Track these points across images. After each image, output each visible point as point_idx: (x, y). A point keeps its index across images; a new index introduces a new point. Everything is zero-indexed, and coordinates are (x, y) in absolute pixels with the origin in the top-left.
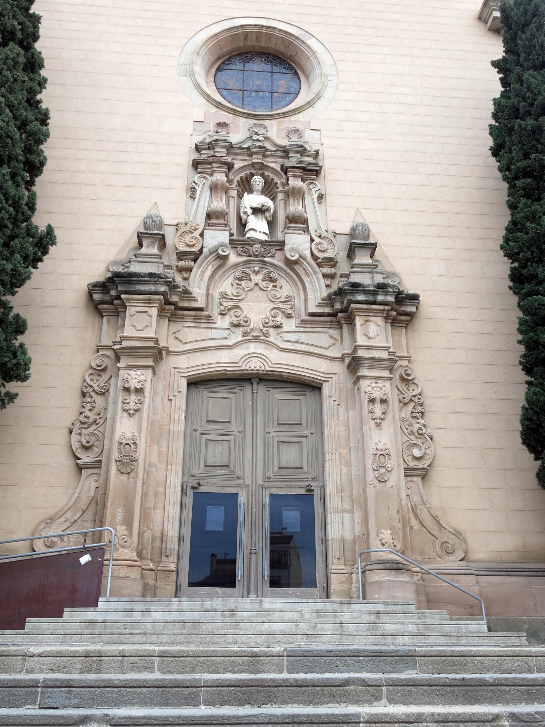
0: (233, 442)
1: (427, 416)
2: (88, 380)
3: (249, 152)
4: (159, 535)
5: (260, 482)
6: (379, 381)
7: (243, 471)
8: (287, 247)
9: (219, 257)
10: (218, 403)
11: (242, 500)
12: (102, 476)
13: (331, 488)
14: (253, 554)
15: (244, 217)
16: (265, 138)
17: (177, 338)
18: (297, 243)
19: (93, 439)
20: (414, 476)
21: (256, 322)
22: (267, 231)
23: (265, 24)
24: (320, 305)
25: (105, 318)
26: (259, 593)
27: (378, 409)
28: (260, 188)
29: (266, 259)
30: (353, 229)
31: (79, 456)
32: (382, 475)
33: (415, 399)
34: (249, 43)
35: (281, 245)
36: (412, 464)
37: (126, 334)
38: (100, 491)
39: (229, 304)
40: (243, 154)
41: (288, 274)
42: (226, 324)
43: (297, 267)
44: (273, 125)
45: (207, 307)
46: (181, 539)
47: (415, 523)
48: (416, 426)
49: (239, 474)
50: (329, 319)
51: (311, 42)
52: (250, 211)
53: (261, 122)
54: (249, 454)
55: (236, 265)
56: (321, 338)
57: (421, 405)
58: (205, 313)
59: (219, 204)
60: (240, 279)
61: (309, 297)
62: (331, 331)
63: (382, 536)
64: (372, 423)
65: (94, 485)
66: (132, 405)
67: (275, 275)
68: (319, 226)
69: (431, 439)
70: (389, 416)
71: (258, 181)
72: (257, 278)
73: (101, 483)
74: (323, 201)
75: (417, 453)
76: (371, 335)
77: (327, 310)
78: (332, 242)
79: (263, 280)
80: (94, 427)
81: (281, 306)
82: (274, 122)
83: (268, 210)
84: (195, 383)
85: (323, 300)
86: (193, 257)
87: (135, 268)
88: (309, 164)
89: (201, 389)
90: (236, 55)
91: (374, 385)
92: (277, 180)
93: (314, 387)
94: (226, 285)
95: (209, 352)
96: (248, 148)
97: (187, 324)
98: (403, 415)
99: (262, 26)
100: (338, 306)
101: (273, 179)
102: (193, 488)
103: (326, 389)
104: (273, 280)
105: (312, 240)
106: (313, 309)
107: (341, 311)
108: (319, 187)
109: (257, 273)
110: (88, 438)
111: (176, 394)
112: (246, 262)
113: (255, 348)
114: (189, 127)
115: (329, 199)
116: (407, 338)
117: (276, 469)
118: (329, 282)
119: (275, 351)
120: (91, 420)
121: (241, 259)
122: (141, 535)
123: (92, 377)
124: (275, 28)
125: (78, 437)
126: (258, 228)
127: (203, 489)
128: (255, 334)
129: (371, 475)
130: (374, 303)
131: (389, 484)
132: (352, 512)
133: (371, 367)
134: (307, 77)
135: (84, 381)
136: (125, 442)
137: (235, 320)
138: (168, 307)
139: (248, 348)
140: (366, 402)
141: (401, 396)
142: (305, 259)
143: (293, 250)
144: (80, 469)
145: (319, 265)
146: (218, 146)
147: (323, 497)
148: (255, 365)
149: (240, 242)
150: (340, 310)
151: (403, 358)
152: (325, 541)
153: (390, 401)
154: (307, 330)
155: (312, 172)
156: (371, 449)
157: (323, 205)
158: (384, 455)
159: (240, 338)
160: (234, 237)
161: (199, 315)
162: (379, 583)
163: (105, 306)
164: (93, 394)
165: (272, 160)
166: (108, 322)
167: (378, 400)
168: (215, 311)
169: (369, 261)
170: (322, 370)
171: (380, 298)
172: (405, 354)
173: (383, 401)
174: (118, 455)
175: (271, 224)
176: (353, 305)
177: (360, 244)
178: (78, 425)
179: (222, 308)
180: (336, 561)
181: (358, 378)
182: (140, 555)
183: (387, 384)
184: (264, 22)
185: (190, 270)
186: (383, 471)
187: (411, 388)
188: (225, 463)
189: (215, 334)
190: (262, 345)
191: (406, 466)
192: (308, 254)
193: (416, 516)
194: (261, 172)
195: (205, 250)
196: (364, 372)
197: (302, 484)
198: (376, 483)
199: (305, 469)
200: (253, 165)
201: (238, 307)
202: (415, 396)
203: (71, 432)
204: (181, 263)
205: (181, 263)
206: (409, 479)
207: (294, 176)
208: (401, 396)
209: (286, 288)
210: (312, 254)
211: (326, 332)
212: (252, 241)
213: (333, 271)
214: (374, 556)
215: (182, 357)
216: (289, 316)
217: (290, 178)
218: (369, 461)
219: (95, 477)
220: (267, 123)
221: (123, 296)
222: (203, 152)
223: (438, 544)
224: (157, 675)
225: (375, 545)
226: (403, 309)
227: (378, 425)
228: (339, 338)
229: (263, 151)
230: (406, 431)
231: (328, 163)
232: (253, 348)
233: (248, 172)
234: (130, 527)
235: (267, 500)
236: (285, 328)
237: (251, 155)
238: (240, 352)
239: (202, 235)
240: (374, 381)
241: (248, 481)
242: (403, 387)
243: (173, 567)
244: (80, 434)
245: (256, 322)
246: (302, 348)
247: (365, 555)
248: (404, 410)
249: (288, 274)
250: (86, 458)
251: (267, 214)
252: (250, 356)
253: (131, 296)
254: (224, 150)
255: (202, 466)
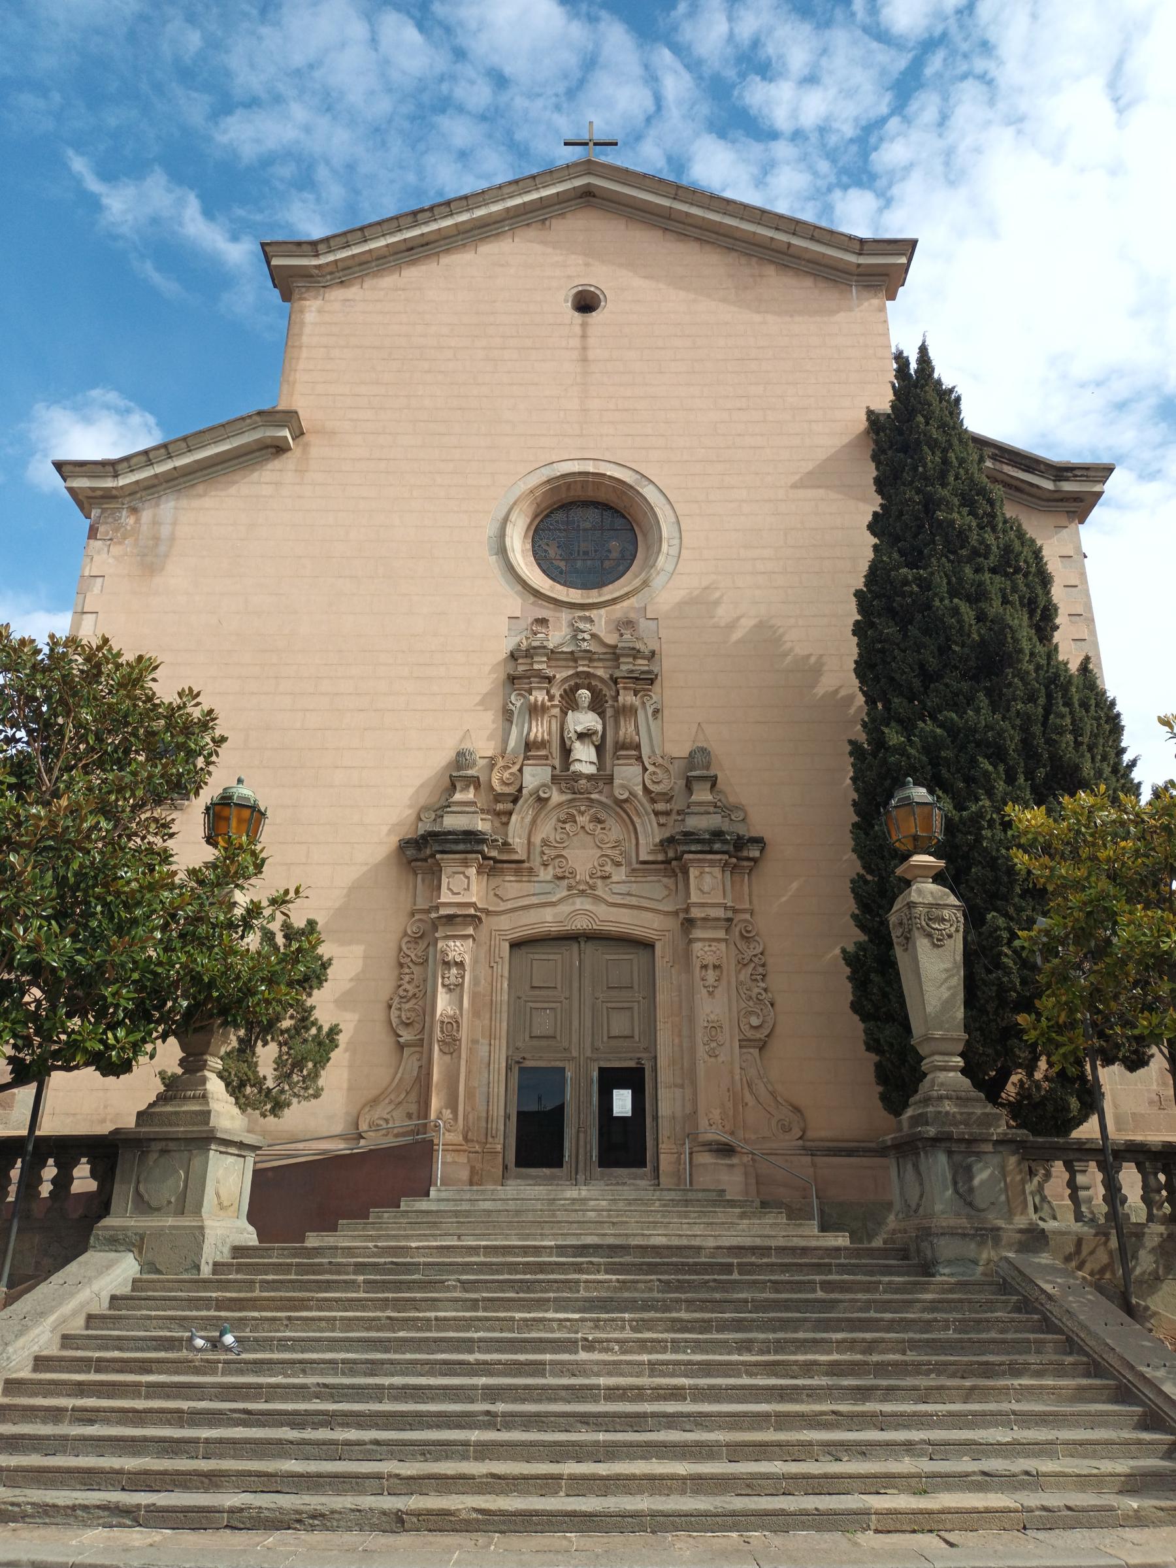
0: (559, 1010)
1: (768, 978)
2: (404, 947)
3: (573, 657)
4: (484, 1115)
5: (589, 1054)
6: (714, 944)
7: (570, 1042)
8: (617, 782)
9: (539, 799)
10: (546, 964)
11: (569, 1074)
12: (425, 1056)
13: (662, 1062)
14: (580, 1135)
15: (568, 743)
16: (592, 635)
17: (496, 895)
18: (628, 775)
19: (413, 1014)
20: (750, 1047)
21: (582, 873)
22: (595, 759)
23: (591, 470)
24: (652, 852)
25: (419, 876)
26: (588, 1174)
27: (711, 975)
28: (586, 705)
29: (593, 796)
30: (692, 755)
31: (400, 1033)
32: (714, 1049)
33: (756, 960)
34: (572, 493)
35: (610, 780)
36: (750, 1034)
37: (443, 900)
38: (424, 1071)
39: (553, 853)
40: (566, 660)
41: (617, 813)
42: (549, 878)
43: (625, 806)
44: (601, 616)
45: (529, 857)
46: (507, 1117)
47: (748, 1097)
48: (757, 990)
49: (566, 1045)
50: (662, 866)
51: (649, 492)
52: (574, 736)
53: (587, 614)
54: (575, 1023)
55: (560, 805)
56: (655, 889)
57: (763, 965)
58: (526, 865)
59: (539, 730)
60: (564, 822)
61: (641, 841)
62: (665, 880)
63: (711, 1116)
64: (704, 991)
65: (416, 1064)
66: (453, 980)
67: (603, 815)
68: (653, 752)
69: (772, 1005)
70: (724, 982)
71: (584, 694)
72: (582, 820)
73: (424, 1062)
74: (659, 716)
75: (755, 1021)
76: (706, 888)
77: (660, 857)
78: (668, 771)
79: (590, 822)
80: (413, 1001)
81: (609, 852)
82: (603, 611)
83: (595, 732)
84: (515, 945)
85: (655, 846)
86: (511, 798)
87: (451, 822)
88: (643, 672)
89: (524, 950)
90: (556, 509)
91: (707, 949)
92: (605, 691)
93: (647, 946)
94: (547, 829)
95: (532, 911)
96: (572, 653)
97: (507, 878)
98: (742, 977)
99: (587, 474)
100: (671, 854)
101: (601, 690)
102: (518, 1062)
103: (658, 946)
104: (600, 822)
105: (645, 769)
106: (644, 856)
107: (676, 859)
108: (655, 698)
109: (582, 813)
110: (408, 1014)
111: (497, 959)
112: (570, 801)
113: (582, 903)
114: (503, 626)
115: (666, 713)
116: (750, 886)
117: (605, 1039)
118: (662, 820)
119: (604, 907)
120: (410, 994)
121: (564, 798)
122: (466, 1117)
123: (410, 945)
124: (605, 475)
125: (398, 1013)
126: (584, 757)
127: (529, 1064)
128: (581, 888)
129: (701, 1051)
130: (711, 852)
131: (720, 1059)
132: (682, 1086)
133: (704, 928)
134: (645, 535)
135: (401, 949)
136: (446, 1020)
137: (559, 872)
138: (486, 862)
139: (574, 903)
140: (698, 969)
141: (740, 956)
142: (635, 796)
143: (623, 786)
144: (401, 1047)
145: (653, 801)
146: (537, 654)
147: (655, 1069)
148: (581, 924)
149: (565, 777)
150: (674, 857)
151: (744, 911)
152: (656, 1118)
153: (725, 966)
154: (639, 879)
155: (646, 681)
156: (701, 1022)
157: (659, 721)
158: (714, 1028)
159: (565, 893)
160: (557, 772)
161: (520, 868)
162: (704, 1165)
163: (419, 863)
164: (410, 964)
165: (600, 664)
166: (423, 880)
167: (711, 966)
168: (536, 862)
169: (710, 798)
170: (655, 926)
171: (717, 846)
172: (747, 906)
173: (715, 967)
174: (439, 1034)
175: (600, 749)
176: (686, 856)
177: (698, 770)
178: (397, 1000)
179: (545, 858)
180: (665, 1139)
181: (691, 941)
182: (466, 1138)
183: (723, 946)
184: (590, 467)
185: (510, 813)
186: (713, 1045)
187: (752, 946)
188: (551, 1033)
189: (537, 888)
190: (590, 900)
191: (742, 1037)
192: (639, 790)
193: (751, 1092)
194: (587, 682)
195: (525, 791)
196: (697, 933)
197: (631, 1055)
198: (706, 1057)
199: (637, 1038)
200: (577, 674)
201: (562, 856)
202: (755, 956)
203: (390, 1007)
204: (500, 807)
205: (500, 807)
206: (744, 1050)
207: (625, 688)
208: (740, 956)
209: (615, 831)
210: (645, 788)
211: (659, 881)
212: (578, 776)
213: (669, 806)
214: (702, 1138)
215: (503, 917)
216: (618, 864)
217: (621, 692)
218: (700, 1035)
219: (417, 1056)
220: (593, 614)
221: (438, 856)
222: (520, 661)
223: (774, 1122)
224: (482, 1259)
225: (703, 1123)
226: (745, 854)
227: (711, 994)
228: (673, 887)
229: (589, 655)
230: (744, 996)
231: (667, 665)
232: (580, 903)
233: (572, 683)
234: (455, 1112)
235: (595, 1074)
236: (615, 878)
237: (575, 660)
238: (565, 909)
239: (520, 770)
240: (707, 944)
241: (575, 1054)
242: (742, 945)
243: (499, 1148)
244: (400, 1009)
245: (582, 873)
246: (634, 901)
247: (692, 1136)
248: (743, 972)
249: (617, 813)
250: (406, 1036)
251: (594, 738)
252: (575, 913)
253: (445, 856)
254: (545, 659)
255: (527, 1038)
